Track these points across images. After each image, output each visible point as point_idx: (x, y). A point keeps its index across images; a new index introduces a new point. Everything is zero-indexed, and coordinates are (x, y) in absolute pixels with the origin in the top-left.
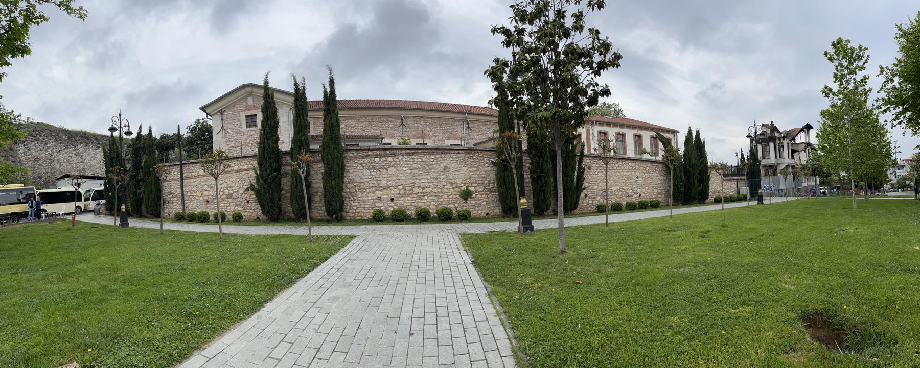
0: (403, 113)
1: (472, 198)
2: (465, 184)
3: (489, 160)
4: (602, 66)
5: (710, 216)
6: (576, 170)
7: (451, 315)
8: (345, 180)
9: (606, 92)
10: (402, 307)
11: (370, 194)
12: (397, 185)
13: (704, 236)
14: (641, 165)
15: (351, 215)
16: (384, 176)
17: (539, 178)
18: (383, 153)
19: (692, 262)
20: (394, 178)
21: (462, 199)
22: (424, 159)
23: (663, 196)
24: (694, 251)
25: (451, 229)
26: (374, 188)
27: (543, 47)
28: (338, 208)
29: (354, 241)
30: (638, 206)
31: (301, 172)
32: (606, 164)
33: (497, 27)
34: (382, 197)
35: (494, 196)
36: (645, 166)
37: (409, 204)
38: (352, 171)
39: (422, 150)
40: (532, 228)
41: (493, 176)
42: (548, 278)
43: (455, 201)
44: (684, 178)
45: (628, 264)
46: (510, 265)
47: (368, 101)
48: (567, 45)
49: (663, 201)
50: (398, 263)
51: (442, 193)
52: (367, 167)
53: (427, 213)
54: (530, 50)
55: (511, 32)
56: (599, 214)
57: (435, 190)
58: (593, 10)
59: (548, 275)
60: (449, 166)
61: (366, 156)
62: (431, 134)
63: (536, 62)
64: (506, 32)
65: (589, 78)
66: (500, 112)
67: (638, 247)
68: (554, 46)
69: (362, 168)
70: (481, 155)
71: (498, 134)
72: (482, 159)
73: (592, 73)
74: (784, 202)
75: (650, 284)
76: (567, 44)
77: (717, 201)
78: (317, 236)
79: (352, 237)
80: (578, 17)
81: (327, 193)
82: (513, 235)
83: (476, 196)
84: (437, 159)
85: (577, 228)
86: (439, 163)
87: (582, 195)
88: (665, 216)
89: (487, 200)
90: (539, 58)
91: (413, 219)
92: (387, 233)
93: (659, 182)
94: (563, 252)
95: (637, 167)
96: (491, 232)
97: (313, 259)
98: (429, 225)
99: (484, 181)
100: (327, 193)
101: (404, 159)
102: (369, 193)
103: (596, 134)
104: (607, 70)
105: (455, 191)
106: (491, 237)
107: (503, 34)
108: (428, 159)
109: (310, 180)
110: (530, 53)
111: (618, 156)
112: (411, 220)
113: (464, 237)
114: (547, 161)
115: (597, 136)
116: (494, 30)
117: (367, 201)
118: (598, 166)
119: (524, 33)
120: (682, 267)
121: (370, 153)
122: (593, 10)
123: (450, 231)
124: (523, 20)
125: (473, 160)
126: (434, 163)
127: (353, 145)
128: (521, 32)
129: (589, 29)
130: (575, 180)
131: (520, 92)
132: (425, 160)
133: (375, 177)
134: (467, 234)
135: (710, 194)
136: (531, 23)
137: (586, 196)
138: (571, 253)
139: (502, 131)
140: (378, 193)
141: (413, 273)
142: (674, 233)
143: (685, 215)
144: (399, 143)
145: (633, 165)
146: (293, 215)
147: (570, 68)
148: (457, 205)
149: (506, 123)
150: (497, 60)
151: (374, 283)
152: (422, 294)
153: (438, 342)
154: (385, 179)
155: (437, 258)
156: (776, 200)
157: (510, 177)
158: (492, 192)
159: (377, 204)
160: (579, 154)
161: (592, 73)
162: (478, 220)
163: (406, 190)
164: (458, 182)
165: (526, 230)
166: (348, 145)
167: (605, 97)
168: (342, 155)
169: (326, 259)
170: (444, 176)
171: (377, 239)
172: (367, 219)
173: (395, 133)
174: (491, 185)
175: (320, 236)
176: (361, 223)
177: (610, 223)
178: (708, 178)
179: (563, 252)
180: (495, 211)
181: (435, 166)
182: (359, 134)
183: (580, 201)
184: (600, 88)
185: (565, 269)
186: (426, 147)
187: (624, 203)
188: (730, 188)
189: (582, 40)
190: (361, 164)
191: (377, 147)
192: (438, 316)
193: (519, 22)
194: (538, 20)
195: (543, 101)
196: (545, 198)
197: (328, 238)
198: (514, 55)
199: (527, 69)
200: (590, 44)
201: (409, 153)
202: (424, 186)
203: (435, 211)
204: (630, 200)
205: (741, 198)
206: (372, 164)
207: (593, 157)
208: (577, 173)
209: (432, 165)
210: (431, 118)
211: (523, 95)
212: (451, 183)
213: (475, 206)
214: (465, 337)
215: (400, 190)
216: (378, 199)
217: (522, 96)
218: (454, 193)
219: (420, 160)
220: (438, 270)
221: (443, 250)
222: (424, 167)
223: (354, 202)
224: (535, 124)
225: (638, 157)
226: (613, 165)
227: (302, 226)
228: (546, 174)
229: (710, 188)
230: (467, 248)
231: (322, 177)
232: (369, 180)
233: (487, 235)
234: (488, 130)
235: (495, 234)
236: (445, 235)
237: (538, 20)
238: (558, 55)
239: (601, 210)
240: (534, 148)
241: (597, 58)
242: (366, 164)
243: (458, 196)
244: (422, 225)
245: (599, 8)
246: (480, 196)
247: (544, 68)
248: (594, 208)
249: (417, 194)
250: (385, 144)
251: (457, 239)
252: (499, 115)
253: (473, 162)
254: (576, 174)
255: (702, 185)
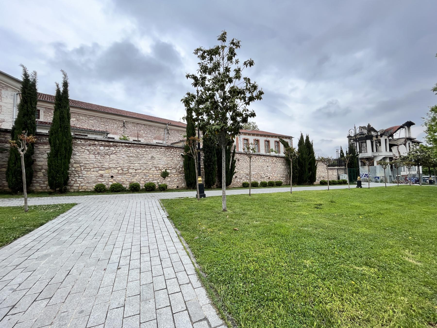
0: (125, 119)
1: (168, 177)
2: (164, 168)
3: (180, 154)
4: (251, 99)
5: (319, 194)
6: (231, 161)
7: (151, 251)
8: (72, 161)
9: (253, 115)
10: (112, 251)
11: (94, 173)
12: (116, 167)
13: (318, 207)
14: (270, 159)
15: (75, 188)
16: (107, 160)
17: (209, 165)
18: (107, 144)
19: (312, 224)
20: (114, 162)
21: (162, 178)
22: (138, 150)
23: (284, 178)
24: (313, 217)
25: (154, 197)
26: (97, 169)
27: (217, 88)
28: (63, 182)
29: (74, 208)
30: (268, 184)
31: (20, 150)
32: (250, 158)
33: (189, 74)
34: (104, 175)
35: (182, 176)
36: (273, 160)
37: (125, 180)
38: (79, 154)
39: (137, 144)
40: (204, 196)
41: (182, 163)
42: (217, 226)
43: (157, 179)
44: (298, 168)
45: (267, 220)
46: (192, 218)
47: (98, 106)
48: (231, 87)
49: (284, 182)
50: (112, 221)
51: (149, 173)
52: (93, 153)
53: (138, 186)
54: (209, 89)
55: (198, 78)
56: (244, 188)
57: (144, 171)
58: (247, 67)
59: (216, 224)
60: (154, 156)
61: (93, 144)
62: (144, 135)
63: (212, 96)
64: (195, 78)
65: (243, 106)
66: (188, 125)
67: (272, 210)
68: (222, 88)
69: (88, 153)
70: (175, 150)
71: (186, 138)
72: (175, 152)
73: (245, 104)
74: (383, 187)
75: (284, 235)
76: (231, 86)
77: (323, 183)
78: (35, 206)
79: (73, 205)
80: (238, 71)
81: (52, 170)
82: (193, 200)
83: (171, 176)
84: (147, 151)
85: (232, 196)
86: (148, 154)
87: (234, 176)
88: (287, 191)
89: (178, 178)
90: (214, 94)
91: (128, 190)
92: (106, 200)
93: (281, 170)
94: (225, 210)
95: (267, 160)
96: (180, 198)
97: (25, 226)
98: (138, 194)
99: (176, 166)
100: (52, 170)
101: (123, 150)
102: (93, 171)
103: (242, 140)
104: (254, 101)
105: (158, 172)
106: (179, 201)
107: (193, 79)
108: (141, 151)
109: (33, 158)
110: (208, 91)
111: (256, 153)
112: (125, 191)
113: (163, 201)
114: (214, 156)
115: (242, 141)
116: (188, 76)
117: (91, 177)
118: (244, 159)
119: (205, 79)
120: (306, 227)
121: (96, 143)
122: (247, 67)
123: (152, 198)
124: (205, 72)
125: (170, 153)
126: (145, 153)
127: (82, 135)
128: (204, 79)
129: (244, 78)
130: (230, 167)
131: (201, 114)
132: (139, 151)
133: (100, 161)
134: (164, 199)
135: (317, 178)
136: (210, 74)
137: (236, 177)
138: (229, 211)
139: (188, 136)
140: (101, 172)
141: (124, 227)
142: (295, 203)
143: (301, 192)
144: (120, 139)
145: (265, 159)
146: (8, 188)
147: (233, 100)
148: (158, 181)
149: (191, 132)
150: (188, 94)
151: (89, 238)
152: (130, 240)
153: (140, 271)
154: (108, 162)
155: (143, 216)
156: (373, 185)
157: (192, 164)
158: (181, 173)
159: (99, 180)
160: (232, 151)
161: (245, 104)
162: (172, 190)
163: (123, 170)
164: (160, 167)
165: (201, 197)
166: (77, 135)
167: (252, 117)
168: (70, 141)
169: (42, 225)
170: (151, 162)
171: (97, 205)
172: (90, 190)
173: (118, 131)
174: (181, 169)
175: (39, 206)
176: (84, 194)
177: (251, 194)
178: (316, 167)
179: (225, 210)
180: (182, 185)
181: (145, 156)
182: (89, 128)
183: (233, 180)
184: (249, 112)
185: (227, 221)
186: (140, 143)
187: (259, 182)
188: (333, 175)
189: (240, 84)
190: (87, 150)
191: (103, 139)
192: (141, 253)
193: (202, 73)
194: (214, 73)
195: (216, 120)
196: (212, 178)
197: (56, 206)
198: (198, 92)
199: (207, 100)
200: (244, 87)
201: (127, 146)
202: (136, 169)
203: (143, 185)
204: (262, 180)
205: (342, 182)
206: (97, 151)
207: (241, 154)
208: (231, 163)
209: (143, 155)
210: (144, 125)
211: (203, 115)
212: (156, 167)
213: (169, 182)
214: (161, 264)
215: (119, 170)
216: (101, 176)
217: (202, 116)
218: (157, 174)
219: (135, 151)
220: (144, 223)
221: (147, 210)
222: (137, 156)
223: (78, 178)
224: (211, 133)
225: (268, 154)
226: (254, 158)
227: (18, 198)
228: (214, 163)
229: (317, 174)
230: (164, 208)
231: (47, 156)
232: (94, 162)
233: (177, 200)
234: (180, 135)
235: (182, 199)
236: (149, 200)
237: (214, 73)
238: (225, 93)
239: (245, 186)
240: (207, 147)
241: (248, 95)
242: (93, 150)
243: (160, 176)
244: (134, 194)
245: (250, 66)
246: (174, 176)
247: (216, 100)
248: (241, 185)
249: (131, 173)
250: (109, 138)
251: (158, 203)
252: (187, 126)
253: (170, 154)
254: (230, 164)
255: (311, 172)
